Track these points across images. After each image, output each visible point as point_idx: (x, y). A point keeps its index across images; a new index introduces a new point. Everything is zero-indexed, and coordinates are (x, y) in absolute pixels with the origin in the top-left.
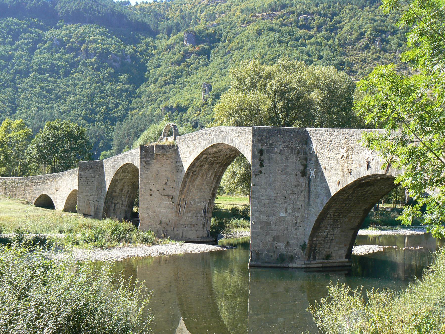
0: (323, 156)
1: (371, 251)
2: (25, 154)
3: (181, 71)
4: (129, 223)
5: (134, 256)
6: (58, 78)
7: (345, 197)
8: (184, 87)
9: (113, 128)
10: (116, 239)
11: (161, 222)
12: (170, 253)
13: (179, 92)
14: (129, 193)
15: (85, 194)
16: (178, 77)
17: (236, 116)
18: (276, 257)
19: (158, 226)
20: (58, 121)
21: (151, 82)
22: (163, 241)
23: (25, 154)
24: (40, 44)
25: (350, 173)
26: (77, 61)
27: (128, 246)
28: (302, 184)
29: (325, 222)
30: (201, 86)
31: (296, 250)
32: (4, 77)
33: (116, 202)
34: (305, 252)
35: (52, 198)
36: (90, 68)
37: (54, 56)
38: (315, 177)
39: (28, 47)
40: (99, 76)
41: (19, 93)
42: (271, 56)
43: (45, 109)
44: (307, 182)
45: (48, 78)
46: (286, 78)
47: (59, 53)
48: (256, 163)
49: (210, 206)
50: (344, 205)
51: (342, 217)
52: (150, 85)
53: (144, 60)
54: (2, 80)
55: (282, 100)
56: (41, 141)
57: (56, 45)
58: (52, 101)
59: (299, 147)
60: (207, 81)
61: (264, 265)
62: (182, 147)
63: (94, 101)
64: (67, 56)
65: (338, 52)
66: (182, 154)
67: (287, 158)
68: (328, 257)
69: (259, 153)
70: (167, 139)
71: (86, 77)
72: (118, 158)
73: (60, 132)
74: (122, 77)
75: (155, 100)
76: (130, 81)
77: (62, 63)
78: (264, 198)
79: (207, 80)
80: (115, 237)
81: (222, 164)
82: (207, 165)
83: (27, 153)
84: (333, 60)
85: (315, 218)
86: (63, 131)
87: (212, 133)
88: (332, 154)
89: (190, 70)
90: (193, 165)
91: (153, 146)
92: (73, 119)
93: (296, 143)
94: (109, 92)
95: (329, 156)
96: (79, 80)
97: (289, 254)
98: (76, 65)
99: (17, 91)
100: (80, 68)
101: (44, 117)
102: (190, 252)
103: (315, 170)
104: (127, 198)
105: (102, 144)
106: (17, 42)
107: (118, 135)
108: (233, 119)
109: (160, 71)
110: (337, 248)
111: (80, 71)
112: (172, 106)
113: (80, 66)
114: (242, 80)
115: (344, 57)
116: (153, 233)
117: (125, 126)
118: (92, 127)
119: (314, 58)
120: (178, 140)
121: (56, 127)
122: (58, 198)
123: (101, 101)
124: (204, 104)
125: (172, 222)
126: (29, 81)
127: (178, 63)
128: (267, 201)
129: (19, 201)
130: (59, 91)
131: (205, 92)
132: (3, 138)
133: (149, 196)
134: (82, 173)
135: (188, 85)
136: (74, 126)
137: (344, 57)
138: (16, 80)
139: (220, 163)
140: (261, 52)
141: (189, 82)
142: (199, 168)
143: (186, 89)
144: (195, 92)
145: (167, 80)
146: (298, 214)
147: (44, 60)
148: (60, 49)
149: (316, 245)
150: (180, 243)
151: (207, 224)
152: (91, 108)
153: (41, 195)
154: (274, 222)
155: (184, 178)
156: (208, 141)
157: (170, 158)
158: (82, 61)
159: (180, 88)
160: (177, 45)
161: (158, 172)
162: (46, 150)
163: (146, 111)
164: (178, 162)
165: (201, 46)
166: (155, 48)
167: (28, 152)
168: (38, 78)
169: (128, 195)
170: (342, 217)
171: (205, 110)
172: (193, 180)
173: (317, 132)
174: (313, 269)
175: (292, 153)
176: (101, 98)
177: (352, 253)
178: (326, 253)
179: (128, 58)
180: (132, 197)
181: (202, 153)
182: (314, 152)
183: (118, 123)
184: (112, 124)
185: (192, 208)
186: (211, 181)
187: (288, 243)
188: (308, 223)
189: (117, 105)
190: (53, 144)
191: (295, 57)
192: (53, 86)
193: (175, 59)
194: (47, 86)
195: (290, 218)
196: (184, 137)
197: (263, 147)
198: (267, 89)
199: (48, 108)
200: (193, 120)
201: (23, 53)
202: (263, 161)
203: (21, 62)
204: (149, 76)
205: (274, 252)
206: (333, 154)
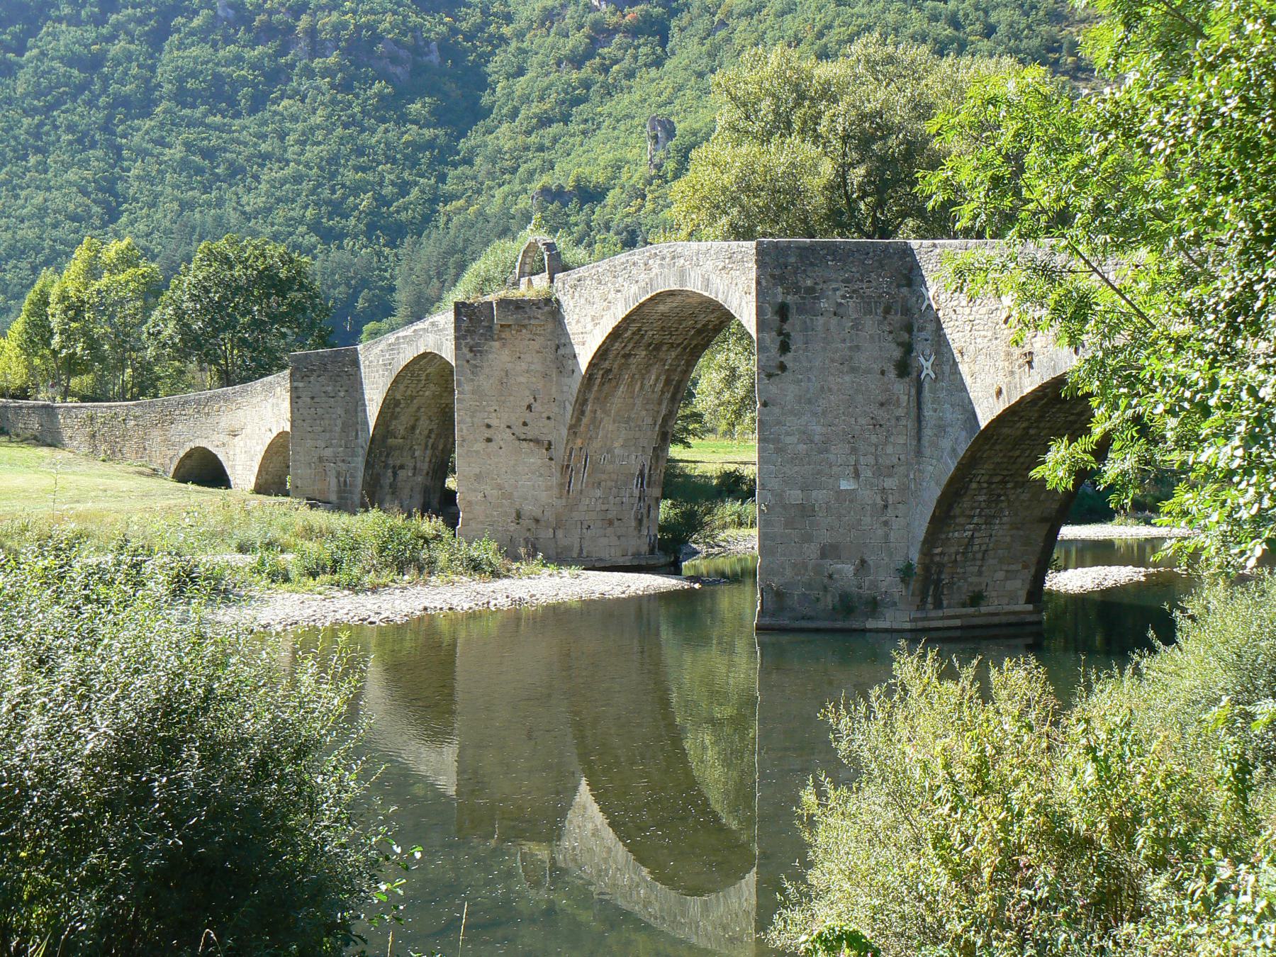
0: (954, 317)
1: (1109, 583)
2: (144, 336)
3: (586, 85)
4: (434, 520)
5: (441, 609)
6: (234, 117)
7: (1019, 432)
8: (594, 130)
9: (396, 255)
10: (392, 563)
11: (519, 516)
12: (542, 600)
13: (581, 145)
14: (433, 436)
15: (309, 443)
16: (578, 101)
17: (735, 211)
18: (829, 601)
19: (513, 527)
20: (231, 241)
21: (499, 118)
22: (524, 568)
23: (144, 336)
24: (180, 20)
25: (1030, 363)
26: (286, 63)
27: (426, 583)
28: (898, 398)
29: (966, 503)
30: (644, 126)
31: (887, 582)
32: (82, 116)
33: (398, 463)
34: (911, 587)
35: (221, 457)
36: (324, 83)
37: (221, 53)
38: (933, 376)
39: (146, 28)
40: (350, 106)
41: (126, 164)
42: (844, 32)
43: (200, 206)
44: (913, 391)
45: (205, 116)
46: (876, 97)
47: (234, 42)
48: (768, 341)
49: (655, 470)
50: (1018, 453)
51: (1012, 488)
52: (497, 127)
53: (478, 55)
54: (77, 126)
55: (863, 161)
56: (184, 299)
57: (226, 19)
58: (218, 184)
59: (888, 293)
60: (660, 111)
61: (797, 624)
62: (571, 304)
63: (340, 177)
64: (256, 52)
65: (1041, 13)
66: (574, 323)
67: (856, 326)
68: (976, 599)
69: (776, 313)
70: (530, 281)
71: (314, 111)
72: (398, 338)
73: (238, 271)
74: (415, 107)
75: (514, 171)
76: (439, 117)
77: (242, 72)
78: (793, 439)
79: (660, 107)
80: (390, 559)
81: (685, 349)
82: (644, 353)
83: (149, 333)
84: (1026, 37)
85: (938, 492)
86: (247, 269)
87: (651, 262)
88: (980, 311)
89: (610, 81)
90: (602, 353)
91: (491, 303)
92: (281, 233)
93: (881, 283)
94: (380, 151)
95: (971, 318)
96: (294, 118)
97: (866, 592)
98: (283, 77)
99: (120, 157)
100: (295, 84)
101: (198, 229)
102: (596, 596)
103: (933, 358)
104: (429, 452)
105: (367, 301)
106: (114, 16)
107: (410, 275)
108: (725, 220)
109: (525, 86)
110: (1000, 575)
111: (297, 92)
112: (561, 187)
113: (295, 78)
114: (747, 106)
115: (1058, 28)
116: (494, 545)
117: (430, 247)
118: (335, 254)
119: (970, 34)
120: (560, 285)
121: (227, 258)
122: (237, 458)
123: (357, 177)
124: (652, 178)
125: (549, 515)
126: (153, 128)
127: (577, 61)
128: (802, 447)
129: (131, 469)
130: (240, 153)
131: (657, 142)
132: (80, 292)
133: (484, 445)
134: (301, 385)
135: (606, 124)
136: (277, 254)
137: (1058, 28)
138: (115, 125)
139: (679, 345)
140: (814, 19)
141: (610, 115)
142: (620, 361)
143: (601, 134)
144: (626, 144)
145: (546, 111)
146: (889, 483)
147: (191, 65)
148: (237, 32)
149: (941, 566)
150: (571, 571)
151: (648, 517)
152: (331, 200)
153: (191, 449)
154: (824, 506)
155: (579, 391)
156: (643, 284)
157: (540, 335)
158: (299, 65)
159: (584, 133)
160: (572, 8)
161: (507, 375)
162: (199, 323)
163: (489, 202)
164: (561, 347)
165: (642, 10)
166: (509, 18)
167: (151, 331)
168: (179, 117)
169: (431, 441)
170: (1012, 488)
171: (657, 194)
172: (604, 395)
173: (938, 251)
174: (939, 634)
175: (871, 312)
176: (357, 169)
177: (1047, 585)
178: (971, 589)
179: (431, 52)
180: (441, 447)
181: (628, 319)
182: (930, 306)
183: (408, 240)
184: (392, 244)
185: (604, 473)
186: (656, 396)
187: (863, 562)
188: (917, 505)
189: (404, 187)
190: (220, 306)
191: (915, 33)
192: (220, 141)
193: (566, 51)
194: (203, 139)
195: (868, 492)
196: (575, 274)
197: (789, 297)
198: (821, 129)
199: (209, 204)
200: (622, 226)
201: (132, 47)
202: (788, 335)
203: (127, 74)
204: (495, 102)
205: (825, 589)
206: (983, 311)
